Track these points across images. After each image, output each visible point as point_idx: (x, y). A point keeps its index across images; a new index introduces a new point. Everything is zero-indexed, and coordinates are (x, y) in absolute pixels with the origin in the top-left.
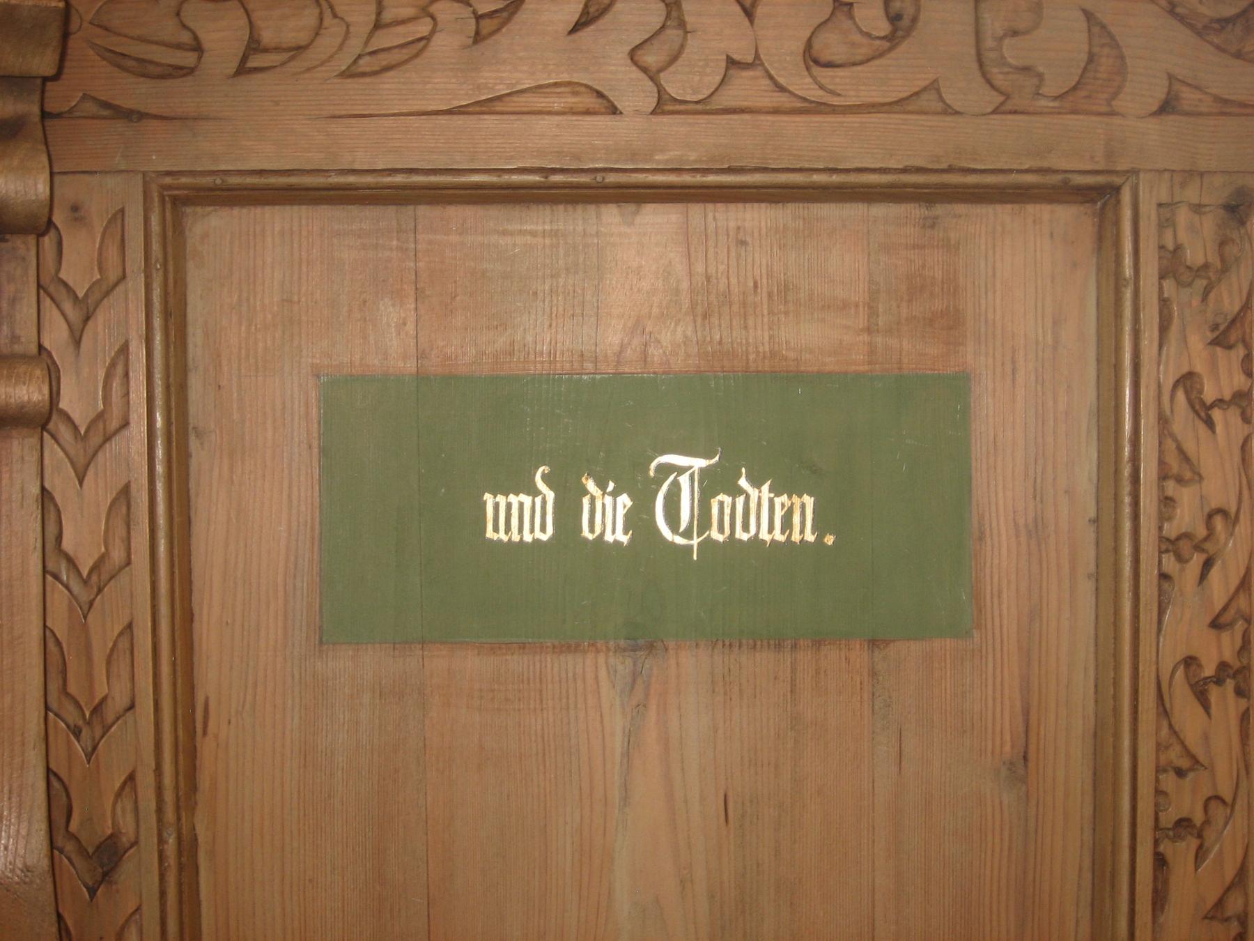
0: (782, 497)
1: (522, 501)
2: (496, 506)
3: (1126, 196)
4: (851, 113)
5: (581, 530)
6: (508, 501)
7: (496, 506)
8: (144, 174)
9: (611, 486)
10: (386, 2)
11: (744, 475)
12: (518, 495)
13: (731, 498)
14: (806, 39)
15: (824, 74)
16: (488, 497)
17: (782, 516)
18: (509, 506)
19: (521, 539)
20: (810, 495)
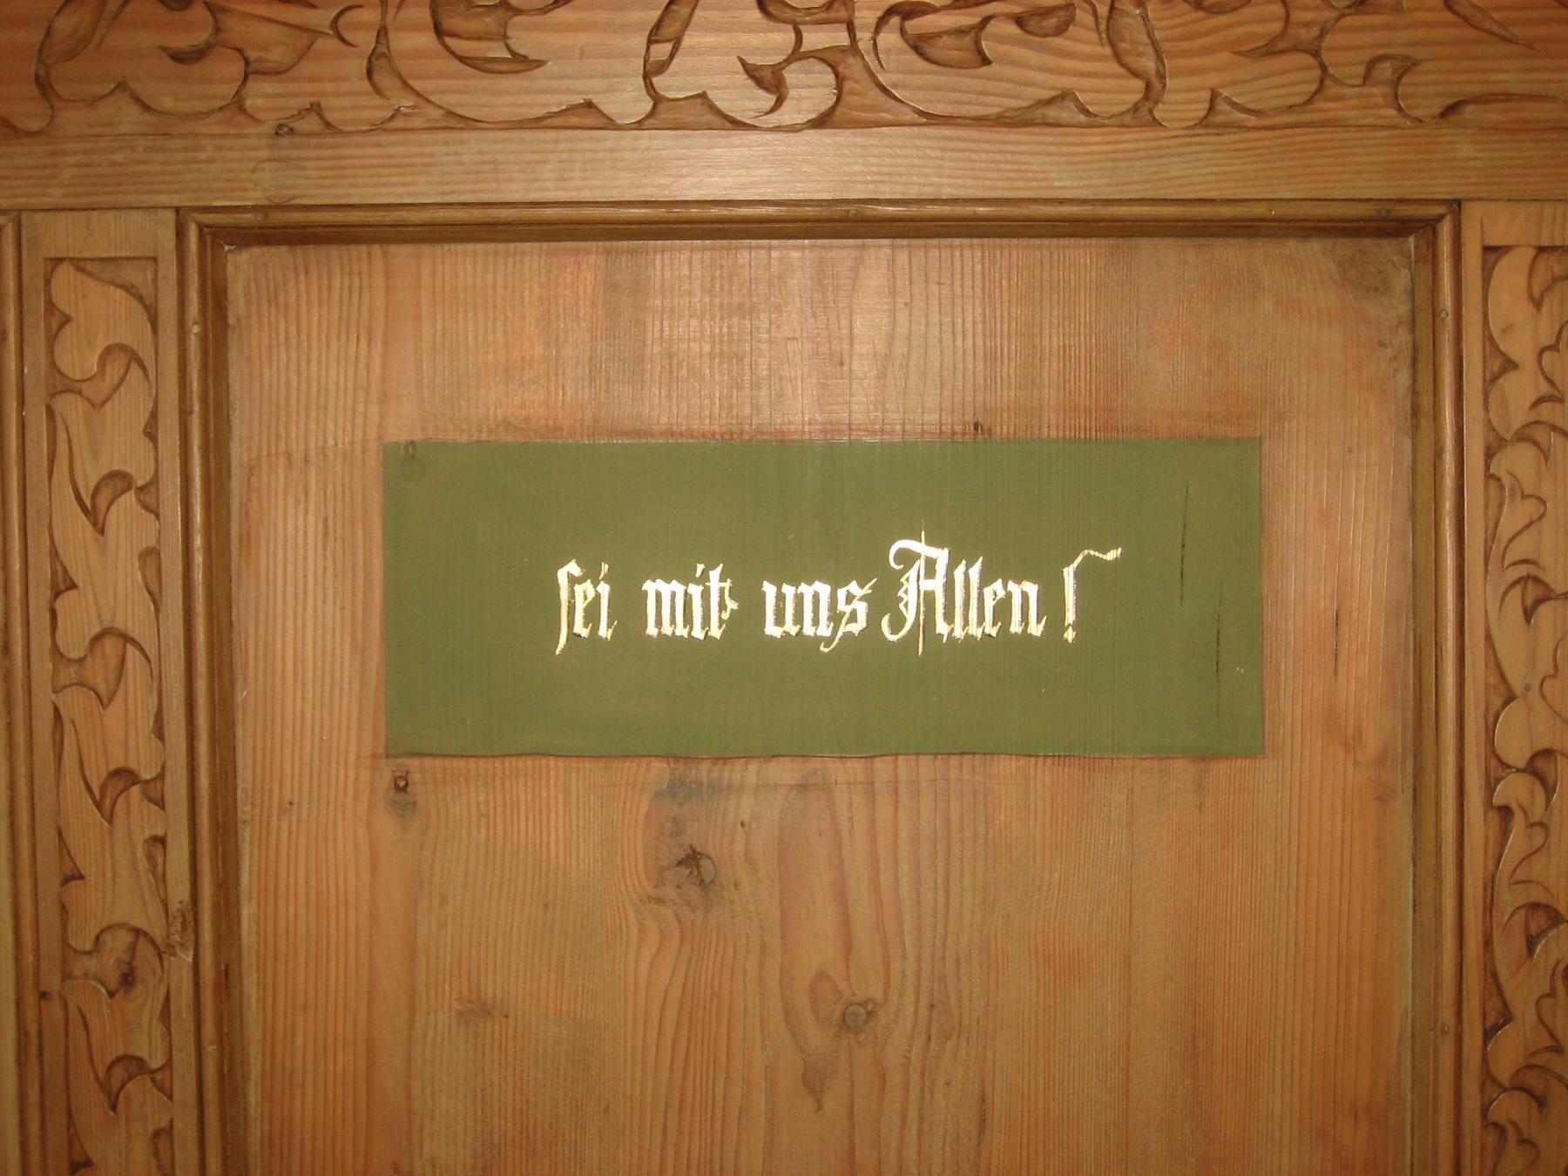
0: (584, 585)
1: (818, 590)
2: (780, 598)
3: (1445, 229)
4: (1123, 221)
5: (763, 626)
6: (799, 592)
7: (780, 598)
8: (177, 210)
9: (605, 568)
10: (700, 3)
11: (1076, 564)
12: (654, 581)
13: (674, 582)
14: (776, 113)
15: (305, 102)
16: (769, 589)
17: (994, 607)
18: (799, 599)
19: (660, 633)
20: (1033, 581)
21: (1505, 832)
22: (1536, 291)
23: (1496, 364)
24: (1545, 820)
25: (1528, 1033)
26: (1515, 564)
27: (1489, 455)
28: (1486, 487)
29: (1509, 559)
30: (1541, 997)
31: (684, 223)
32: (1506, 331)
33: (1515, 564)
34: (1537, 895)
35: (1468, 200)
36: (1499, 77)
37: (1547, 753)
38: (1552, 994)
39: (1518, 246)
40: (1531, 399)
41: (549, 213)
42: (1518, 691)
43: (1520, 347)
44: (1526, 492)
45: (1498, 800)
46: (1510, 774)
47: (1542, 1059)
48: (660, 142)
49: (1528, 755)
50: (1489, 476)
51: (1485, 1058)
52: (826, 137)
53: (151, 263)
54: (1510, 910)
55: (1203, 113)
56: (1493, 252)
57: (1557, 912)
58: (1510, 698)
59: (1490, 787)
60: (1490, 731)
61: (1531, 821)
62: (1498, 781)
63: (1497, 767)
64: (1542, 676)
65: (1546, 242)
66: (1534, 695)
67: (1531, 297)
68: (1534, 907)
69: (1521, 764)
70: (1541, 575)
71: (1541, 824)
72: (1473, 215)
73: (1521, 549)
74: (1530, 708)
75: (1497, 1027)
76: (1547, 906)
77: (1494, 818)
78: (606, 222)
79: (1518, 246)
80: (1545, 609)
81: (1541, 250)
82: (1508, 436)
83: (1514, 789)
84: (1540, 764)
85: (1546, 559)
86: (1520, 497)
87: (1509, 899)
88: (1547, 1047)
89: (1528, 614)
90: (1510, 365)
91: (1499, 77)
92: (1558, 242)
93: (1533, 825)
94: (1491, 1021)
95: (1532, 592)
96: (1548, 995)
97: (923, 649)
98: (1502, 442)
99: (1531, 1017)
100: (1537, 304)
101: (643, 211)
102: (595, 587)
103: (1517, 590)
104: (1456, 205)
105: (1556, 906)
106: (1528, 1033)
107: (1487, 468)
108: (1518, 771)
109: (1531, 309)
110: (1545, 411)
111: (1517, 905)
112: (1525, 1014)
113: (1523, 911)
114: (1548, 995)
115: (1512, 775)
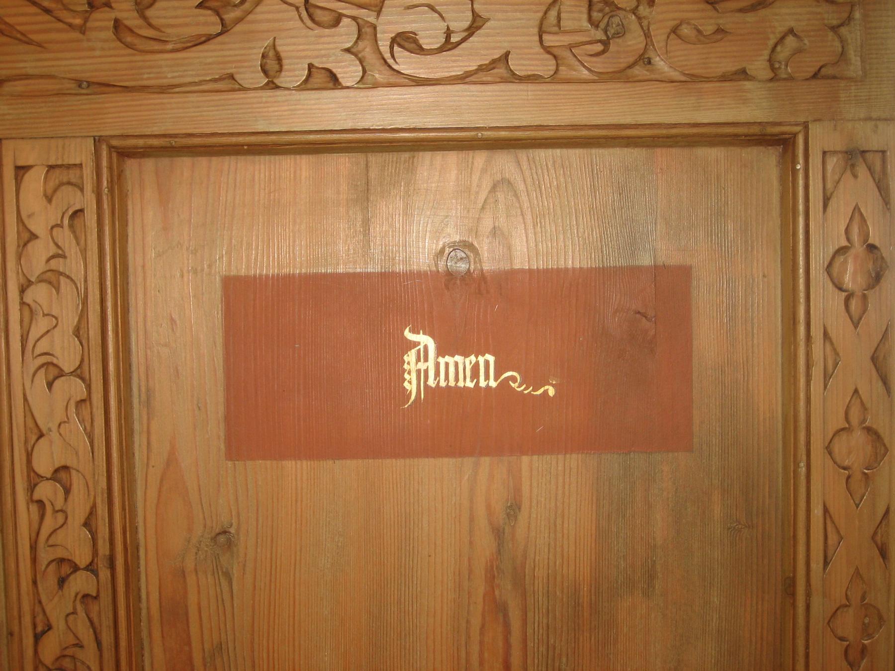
1: (447, 361)
20: (493, 355)
21: (42, 517)
22: (49, 192)
23: (26, 236)
24: (64, 508)
25: (61, 636)
26: (39, 355)
27: (22, 291)
28: (21, 310)
29: (38, 351)
30: (68, 615)
31: (287, 145)
32: (29, 216)
33: (39, 355)
34: (60, 553)
35: (7, 139)
36: (21, 65)
37: (65, 468)
38: (74, 612)
39: (36, 165)
40: (44, 259)
41: (312, 137)
42: (45, 431)
43: (38, 226)
44: (46, 312)
45: (36, 496)
46: (42, 481)
47: (69, 652)
48: (310, 98)
49: (52, 470)
50: (23, 303)
51: (36, 652)
52: (814, 83)
53: (828, 156)
54: (46, 563)
55: (552, 73)
56: (21, 170)
57: (76, 565)
58: (41, 435)
59: (31, 488)
60: (29, 456)
61: (57, 509)
62: (35, 485)
63: (33, 480)
64: (59, 422)
65: (52, 162)
66: (55, 435)
67: (45, 195)
68: (61, 561)
69: (49, 476)
70: (55, 361)
71: (61, 511)
72: (815, 130)
73: (42, 347)
74: (51, 442)
75: (44, 633)
76: (69, 560)
77: (34, 508)
78: (301, 143)
79: (36, 165)
80: (58, 384)
81: (51, 167)
82: (33, 279)
83: (45, 491)
84: (63, 475)
85: (57, 351)
86: (42, 315)
87: (45, 556)
88: (73, 645)
89: (50, 385)
90: (34, 236)
91: (21, 65)
92: (59, 163)
93: (58, 511)
94: (39, 629)
95: (53, 372)
96: (73, 613)
97: (424, 396)
98: (30, 283)
99: (62, 625)
100: (49, 199)
101: (434, 134)
102: (477, 358)
103: (43, 370)
104: (806, 126)
105: (74, 560)
106: (61, 636)
107: (22, 298)
108: (47, 479)
109: (44, 201)
110: (53, 264)
111: (50, 559)
112: (59, 624)
113: (54, 564)
114: (73, 613)
115: (44, 482)
